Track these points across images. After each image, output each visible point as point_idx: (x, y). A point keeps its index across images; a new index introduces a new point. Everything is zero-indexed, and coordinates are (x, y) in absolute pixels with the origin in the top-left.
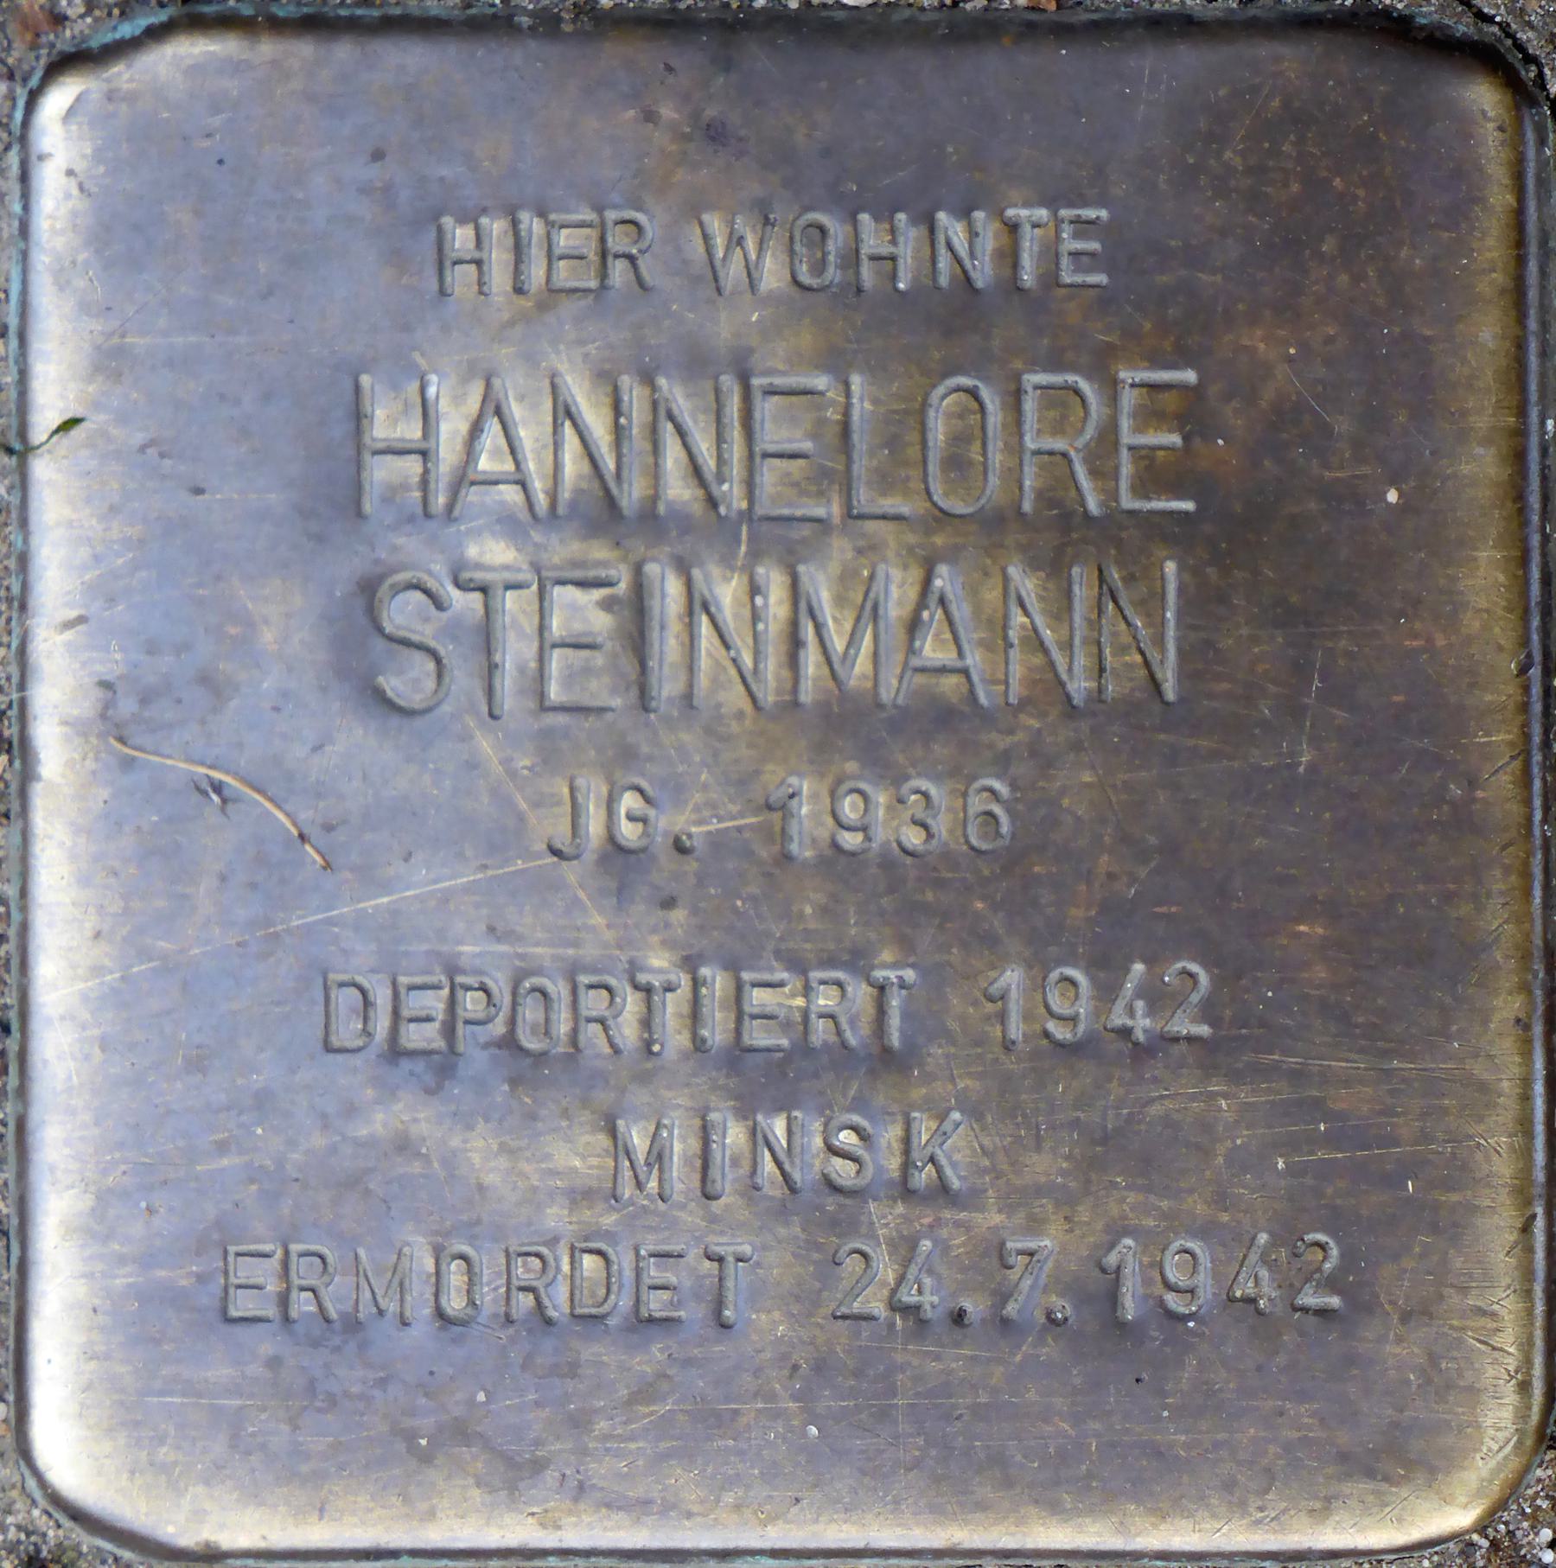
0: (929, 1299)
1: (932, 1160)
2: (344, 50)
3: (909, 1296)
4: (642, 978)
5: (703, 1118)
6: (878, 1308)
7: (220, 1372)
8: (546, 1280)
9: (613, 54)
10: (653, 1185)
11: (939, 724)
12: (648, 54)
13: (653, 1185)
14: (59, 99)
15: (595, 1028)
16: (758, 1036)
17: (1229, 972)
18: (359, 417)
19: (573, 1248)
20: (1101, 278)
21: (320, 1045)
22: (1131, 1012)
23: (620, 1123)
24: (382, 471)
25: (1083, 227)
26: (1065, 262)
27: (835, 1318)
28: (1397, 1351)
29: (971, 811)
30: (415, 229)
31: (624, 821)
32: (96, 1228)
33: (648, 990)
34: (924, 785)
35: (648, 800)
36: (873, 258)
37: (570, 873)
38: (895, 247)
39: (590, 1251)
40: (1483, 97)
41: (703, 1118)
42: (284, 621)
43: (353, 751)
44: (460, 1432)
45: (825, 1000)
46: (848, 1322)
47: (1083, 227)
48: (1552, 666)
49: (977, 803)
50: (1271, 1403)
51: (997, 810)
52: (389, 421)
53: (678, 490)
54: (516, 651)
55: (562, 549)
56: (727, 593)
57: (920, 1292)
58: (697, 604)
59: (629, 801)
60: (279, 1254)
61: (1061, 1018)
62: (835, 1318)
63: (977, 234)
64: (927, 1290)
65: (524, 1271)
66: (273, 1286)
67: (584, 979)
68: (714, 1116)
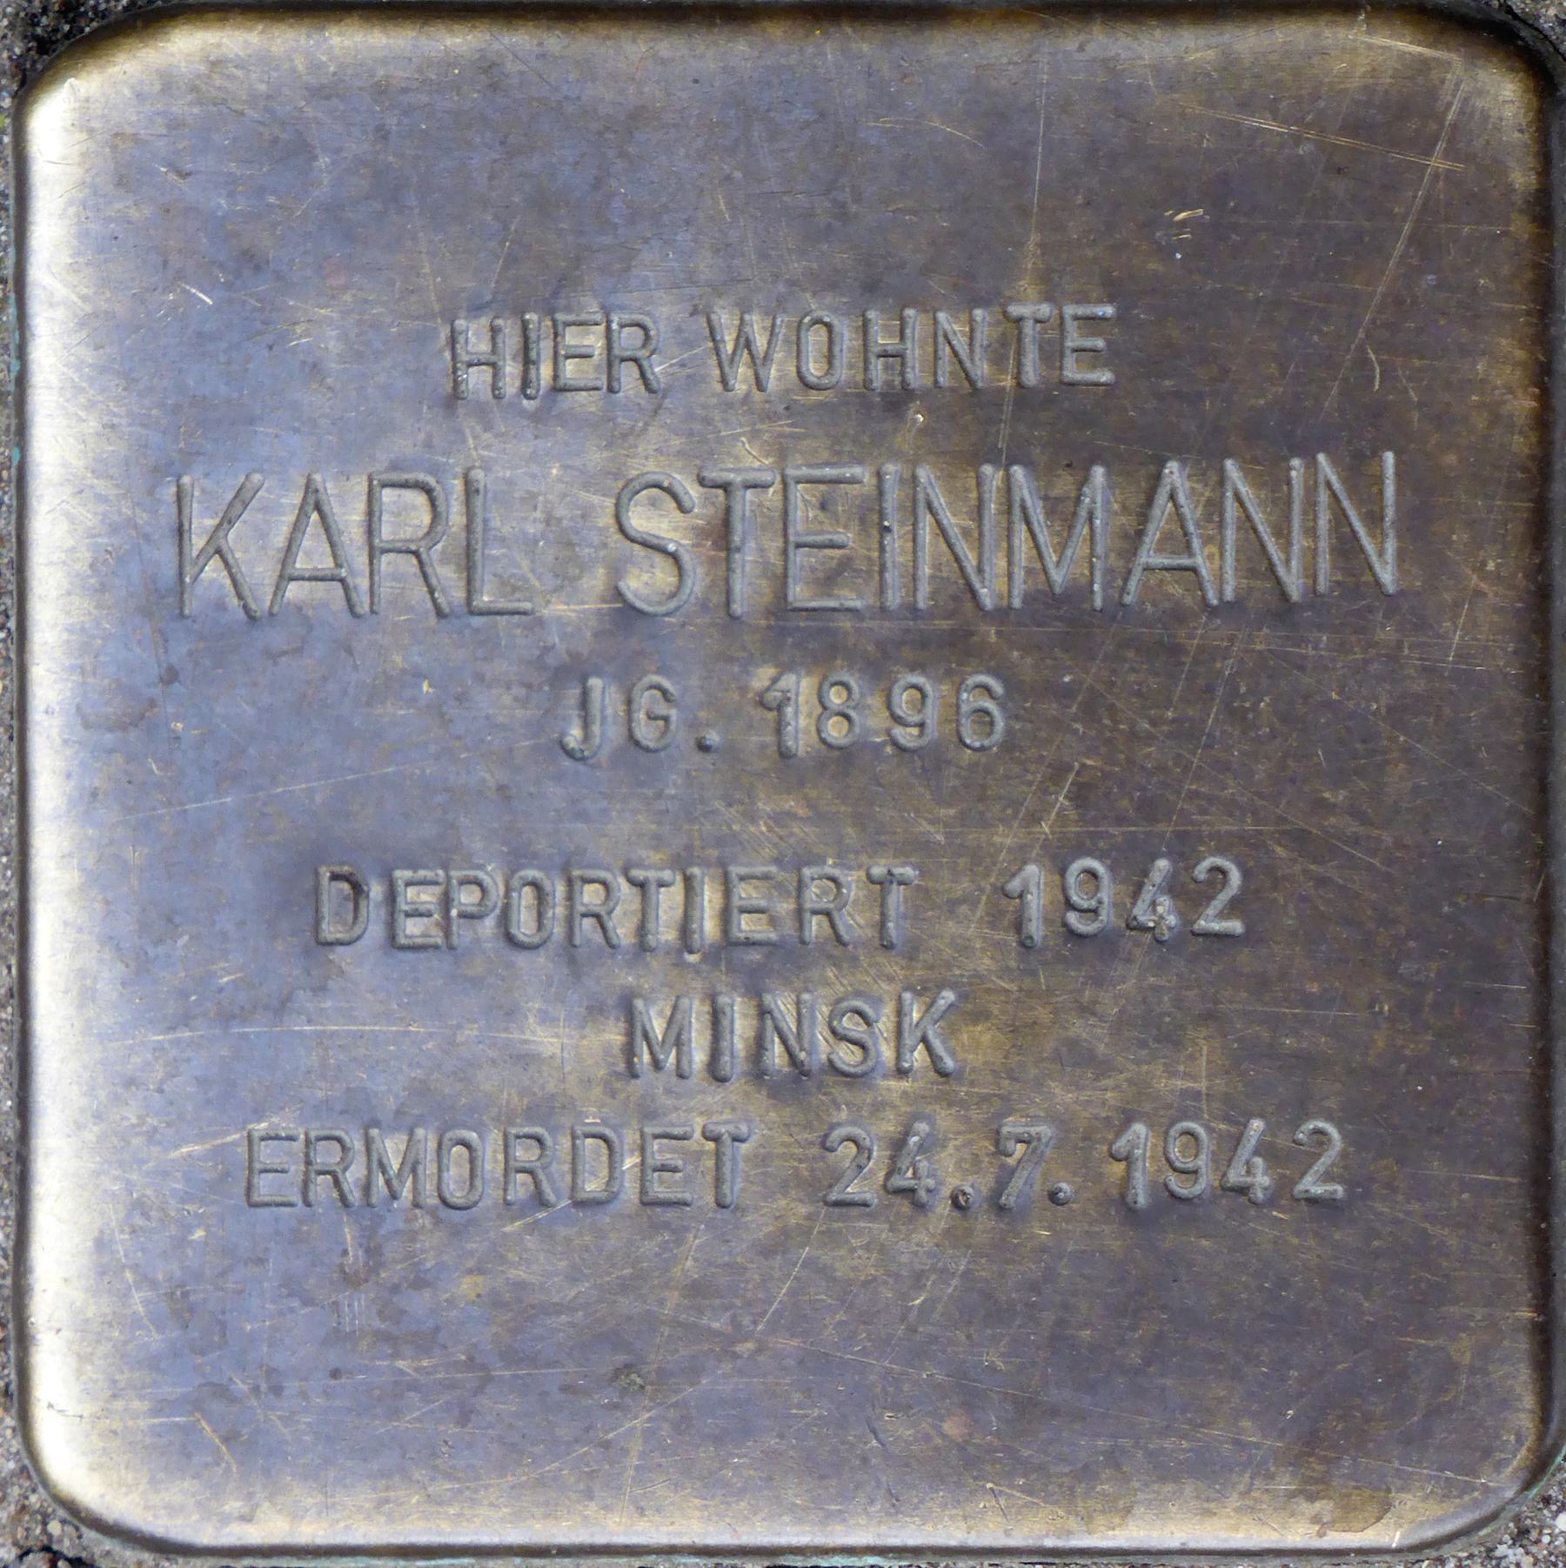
1: (924, 1040)
4: (638, 874)
5: (714, 1003)
10: (406, 1192)
11: (947, 635)
13: (406, 1192)
15: (588, 923)
16: (746, 925)
17: (1009, 745)
20: (1105, 376)
21: (313, 942)
23: (639, 1004)
25: (1091, 323)
26: (1071, 326)
29: (965, 708)
33: (642, 885)
34: (918, 679)
41: (714, 1003)
47: (1091, 323)
49: (969, 701)
51: (990, 705)
65: (524, 1154)
66: (296, 1169)
68: (723, 1000)
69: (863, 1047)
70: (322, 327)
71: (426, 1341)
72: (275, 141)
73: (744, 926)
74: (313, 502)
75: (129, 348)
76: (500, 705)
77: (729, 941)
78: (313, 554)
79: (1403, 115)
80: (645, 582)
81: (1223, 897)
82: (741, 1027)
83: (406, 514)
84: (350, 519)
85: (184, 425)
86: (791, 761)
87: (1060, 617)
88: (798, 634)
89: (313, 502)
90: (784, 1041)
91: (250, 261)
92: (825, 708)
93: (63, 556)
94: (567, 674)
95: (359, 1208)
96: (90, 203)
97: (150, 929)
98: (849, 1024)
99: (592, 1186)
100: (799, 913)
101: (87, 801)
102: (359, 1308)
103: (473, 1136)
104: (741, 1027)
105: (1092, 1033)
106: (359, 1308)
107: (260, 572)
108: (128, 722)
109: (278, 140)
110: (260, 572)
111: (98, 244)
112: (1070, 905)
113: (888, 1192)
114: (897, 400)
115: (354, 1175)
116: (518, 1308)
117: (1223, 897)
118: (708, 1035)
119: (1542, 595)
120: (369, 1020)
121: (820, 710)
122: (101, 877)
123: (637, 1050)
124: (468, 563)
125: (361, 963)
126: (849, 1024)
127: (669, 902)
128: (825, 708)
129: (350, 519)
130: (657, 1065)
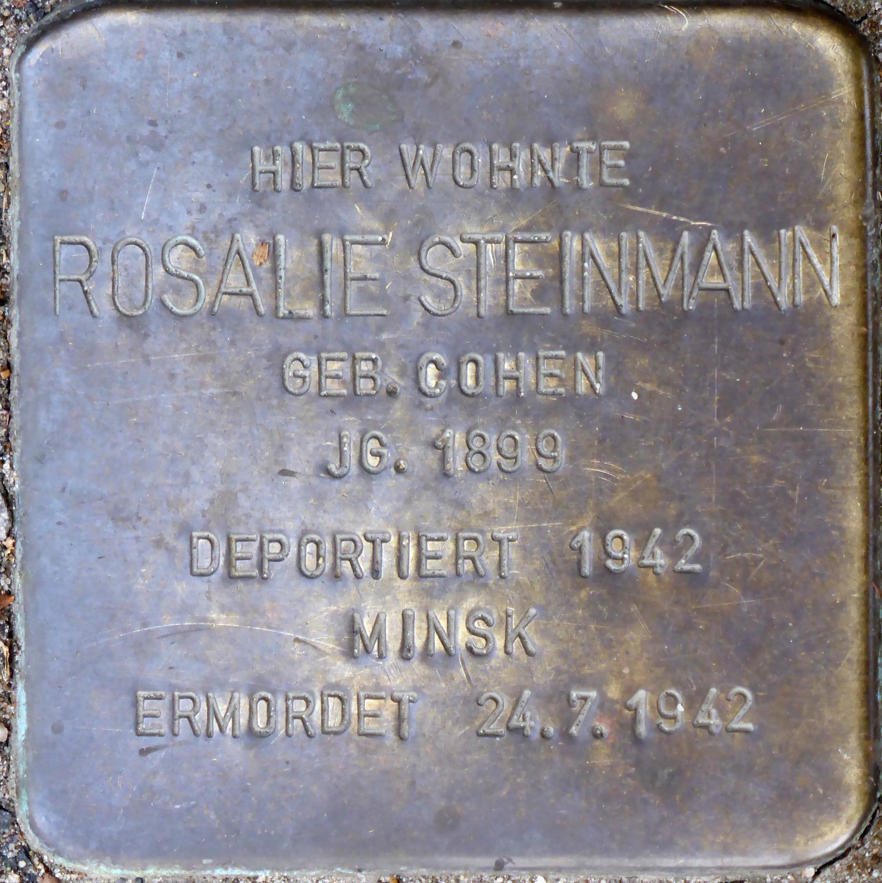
0: (529, 723)
3: (516, 722)
6: (502, 730)
8: (309, 712)
19: (322, 694)
22: (653, 555)
27: (479, 735)
31: (369, 456)
35: (382, 444)
36: (261, 173)
37: (275, 480)
39: (334, 696)
46: (486, 738)
48: (879, 339)
50: (666, 771)
57: (524, 719)
59: (373, 444)
60: (168, 698)
61: (615, 558)
62: (479, 735)
64: (528, 719)
66: (164, 714)
67: (269, 536)
69: (485, 637)
72: (233, 343)
73: (429, 548)
81: (690, 553)
86: (451, 479)
87: (664, 323)
90: (440, 638)
92: (470, 449)
98: (479, 626)
99: (333, 721)
100: (457, 555)
103: (269, 696)
112: (609, 556)
113: (693, 725)
115: (200, 718)
117: (690, 553)
118: (599, 261)
121: (467, 450)
123: (356, 645)
126: (479, 626)
128: (470, 449)
130: (367, 651)
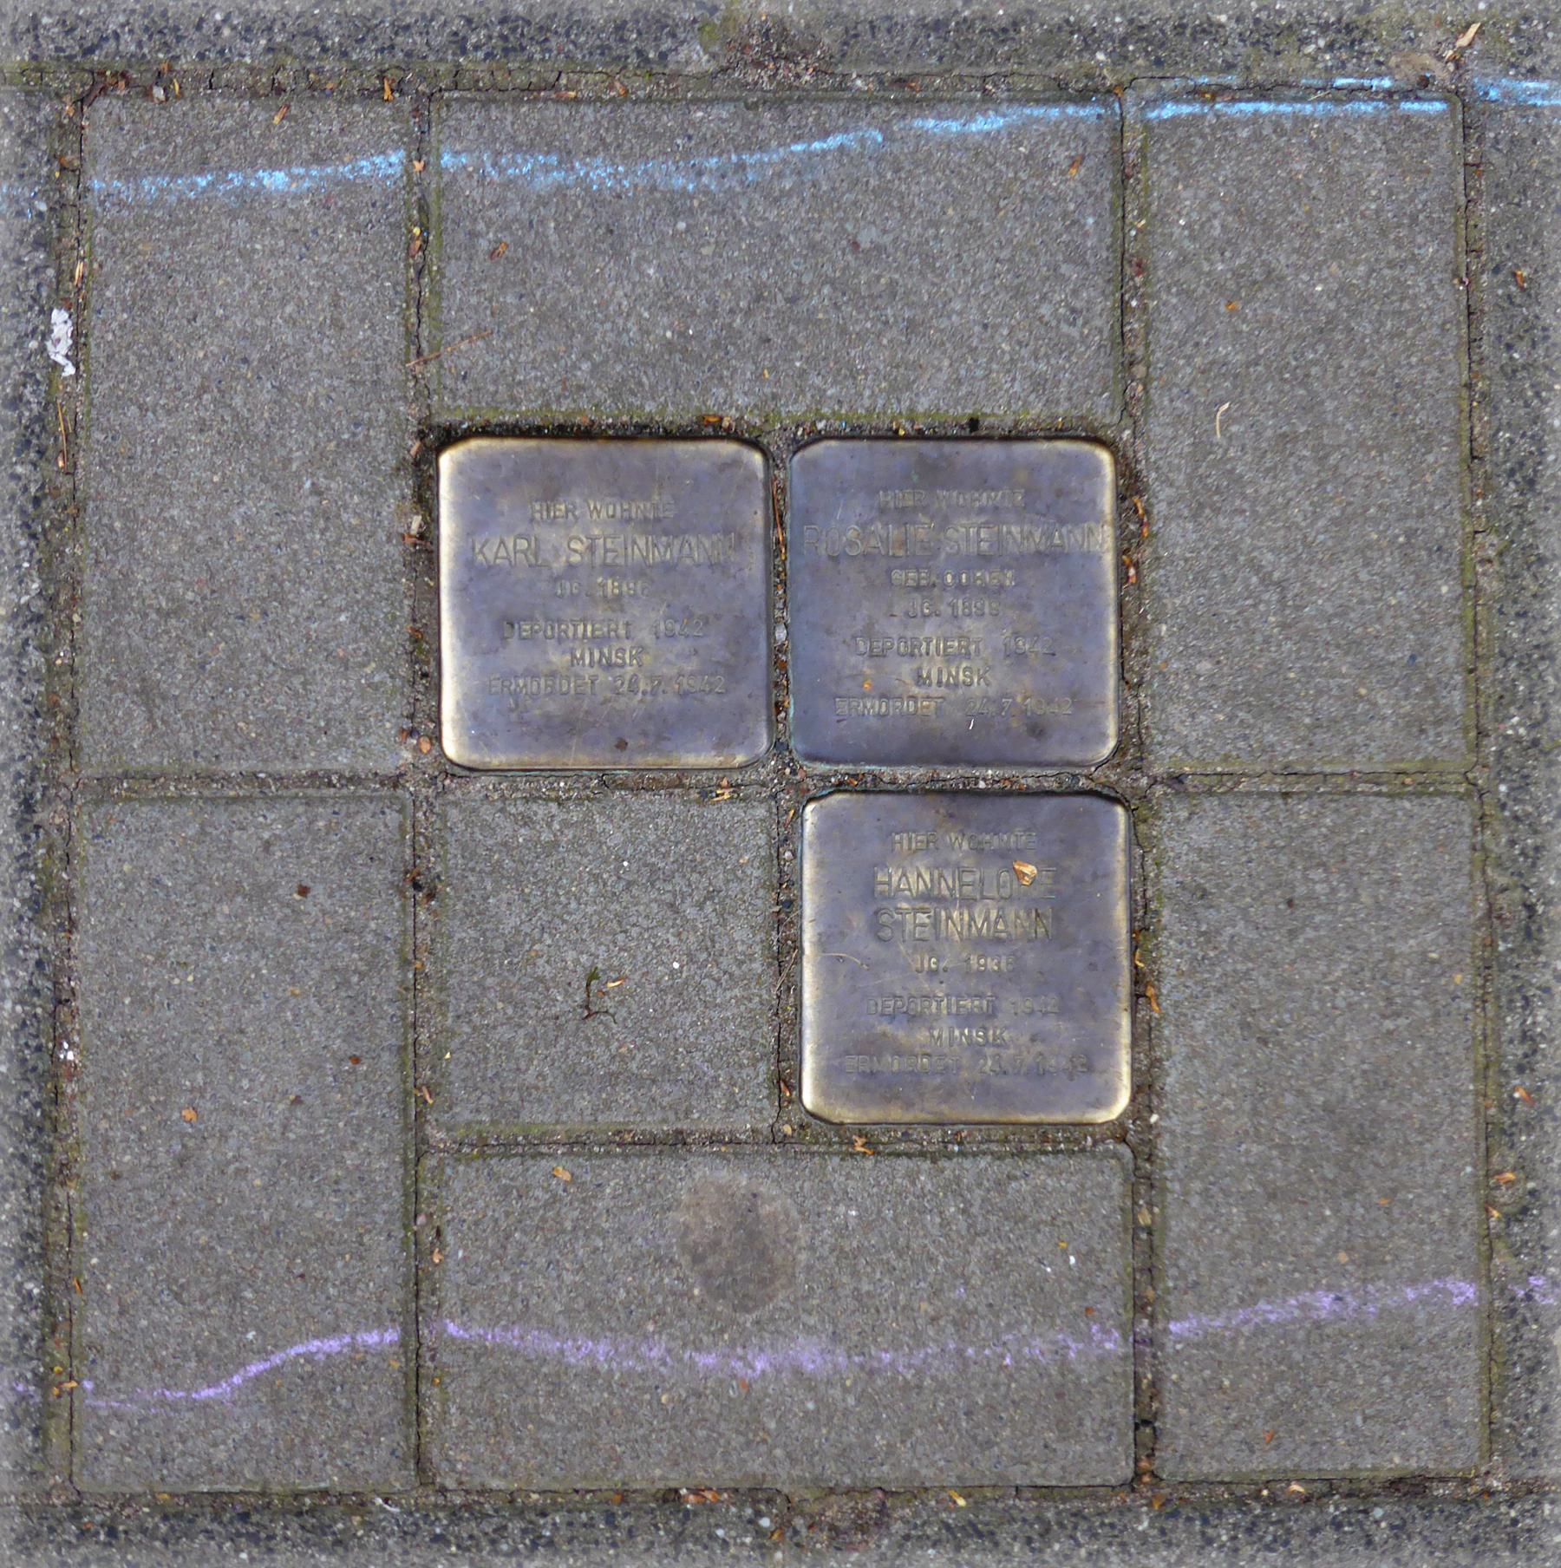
2: (872, 797)
7: (844, 1084)
9: (929, 798)
12: (938, 798)
14: (810, 808)
18: (874, 876)
24: (880, 888)
28: (1098, 1080)
30: (887, 835)
32: (817, 1052)
38: (638, 509)
40: (1120, 810)
42: (859, 921)
43: (872, 948)
44: (897, 1097)
45: (887, 1357)
52: (881, 877)
53: (946, 892)
54: (909, 927)
55: (919, 905)
56: (955, 914)
58: (949, 917)
63: (974, 423)
70: (504, 504)
71: (527, 723)
74: (502, 542)
75: (460, 508)
76: (543, 586)
77: (594, 637)
78: (502, 553)
79: (735, 463)
80: (576, 558)
82: (597, 655)
83: (523, 544)
84: (510, 546)
85: (472, 527)
88: (611, 570)
89: (502, 542)
91: (488, 490)
93: (1373, 16)
94: (556, 579)
95: (515, 695)
96: (453, 478)
97: (468, 634)
101: (453, 607)
102: (514, 716)
104: (597, 655)
105: (672, 657)
106: (514, 716)
107: (490, 556)
108: (461, 590)
109: (494, 464)
110: (490, 556)
111: (455, 486)
114: (629, 520)
116: (548, 717)
119: (872, 1511)
120: (515, 655)
122: (456, 623)
124: (536, 556)
125: (514, 642)
127: (581, 628)
129: (510, 546)
